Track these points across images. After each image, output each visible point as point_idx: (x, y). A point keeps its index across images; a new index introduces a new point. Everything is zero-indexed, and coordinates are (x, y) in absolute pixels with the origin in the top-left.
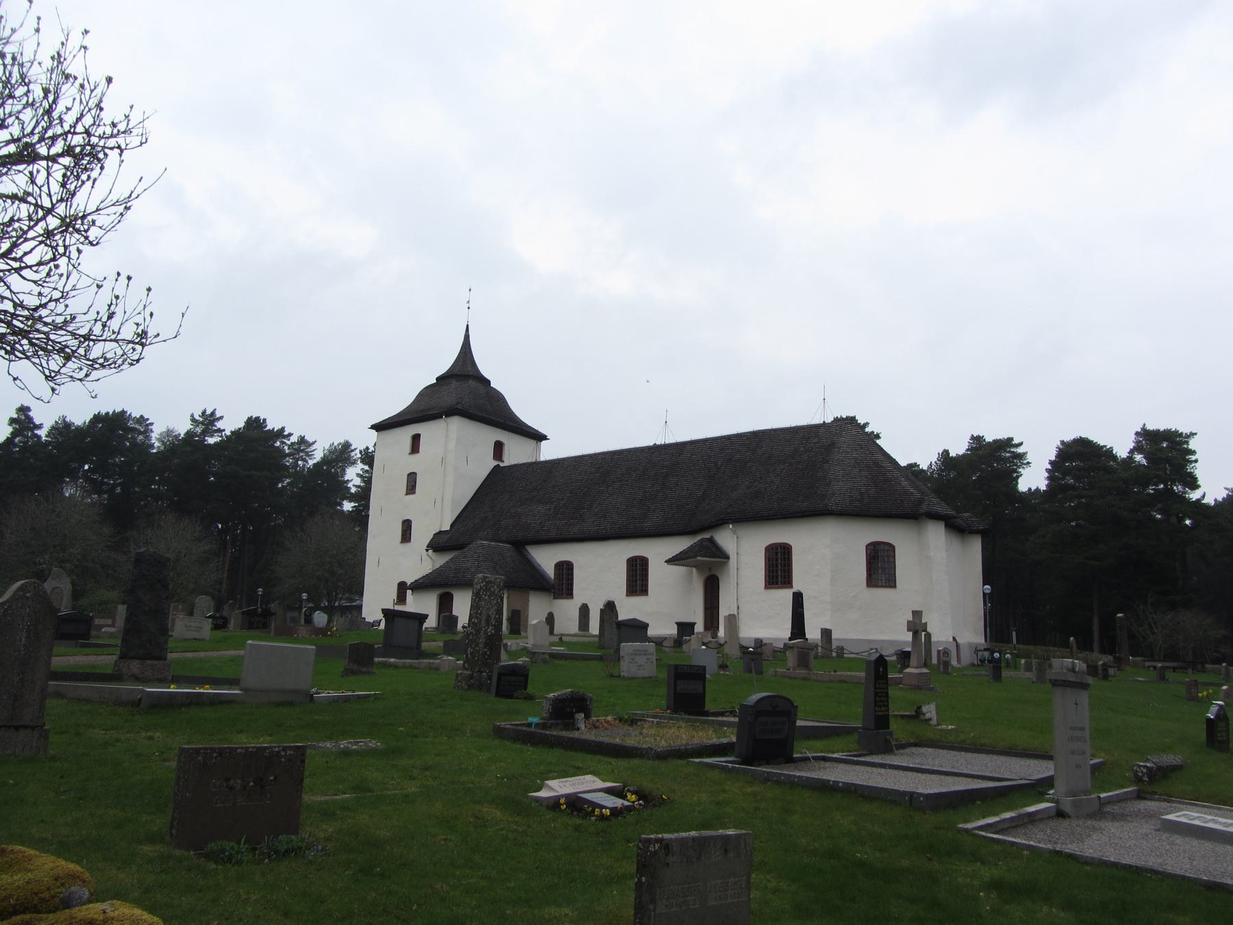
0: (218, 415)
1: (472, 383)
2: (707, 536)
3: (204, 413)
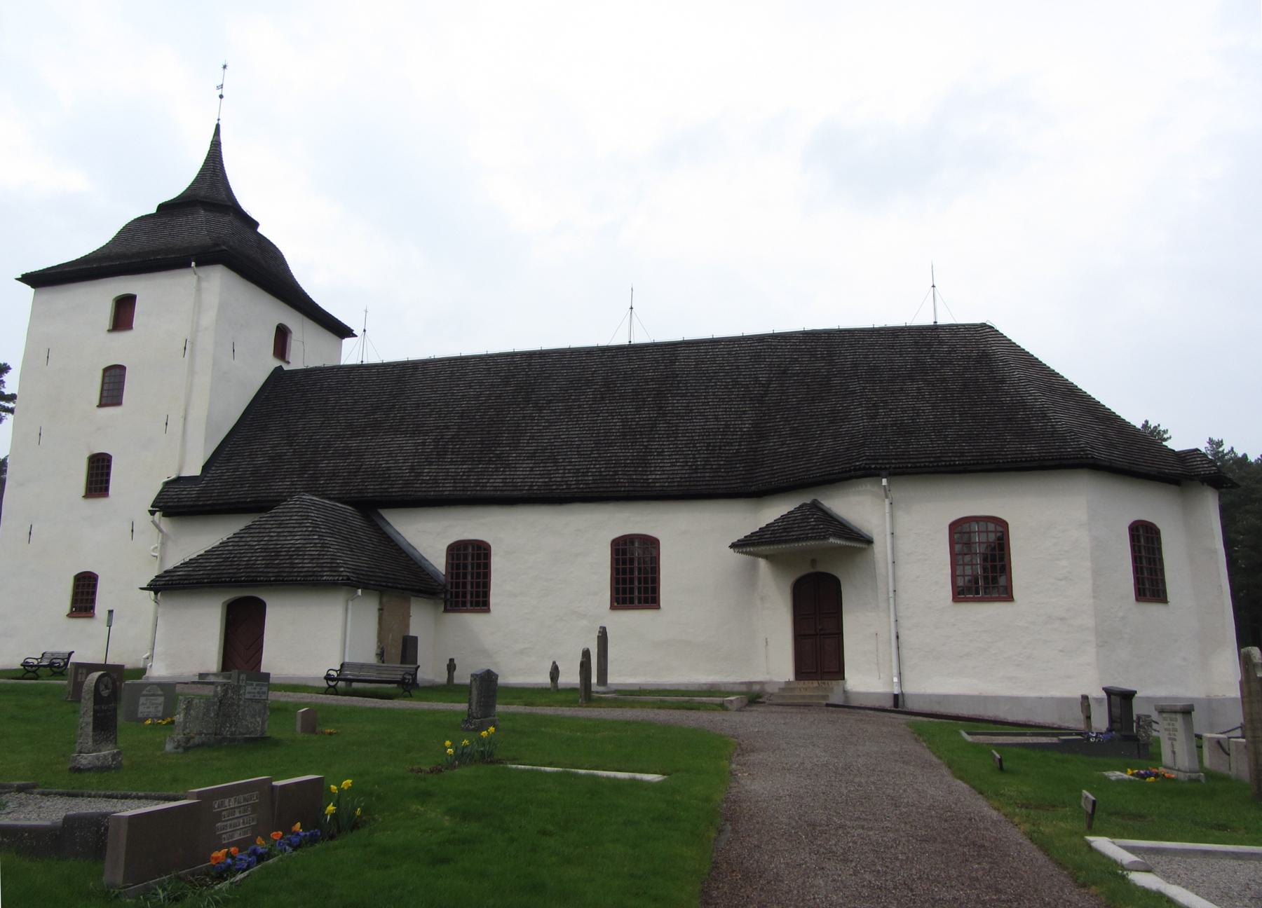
1: (228, 219)
2: (806, 498)
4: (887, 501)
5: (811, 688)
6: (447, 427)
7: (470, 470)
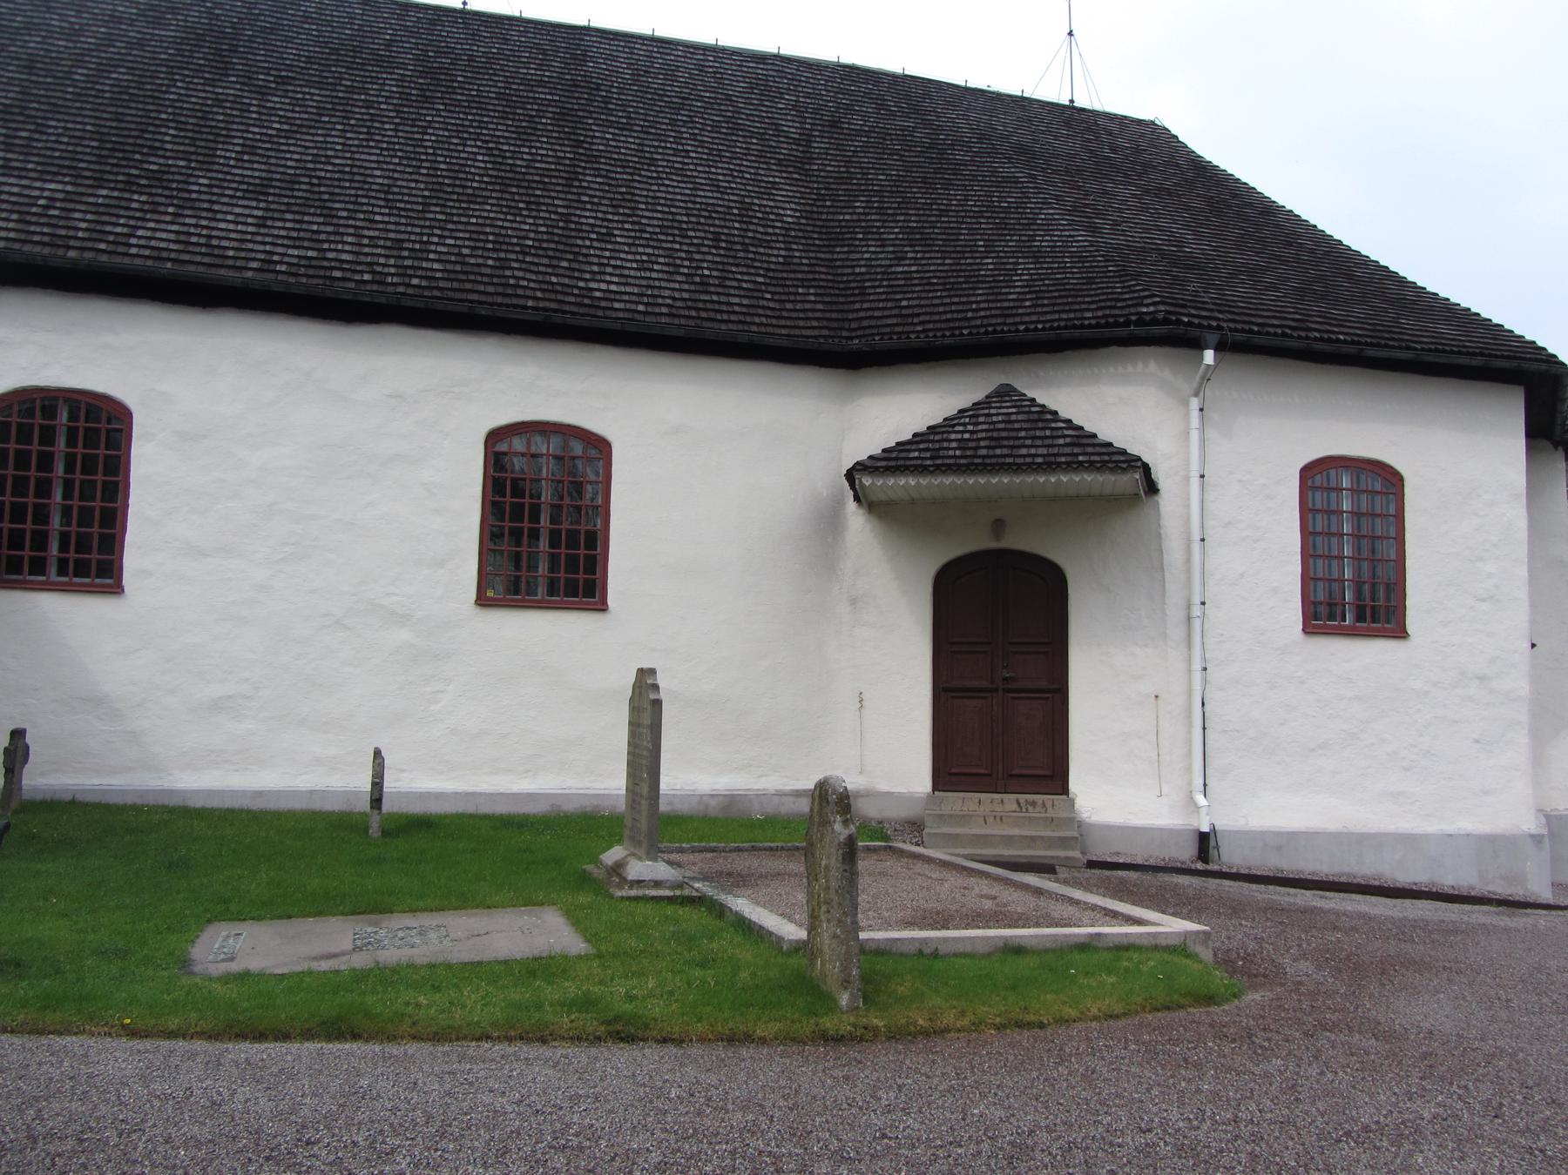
4: (1195, 403)
5: (995, 816)
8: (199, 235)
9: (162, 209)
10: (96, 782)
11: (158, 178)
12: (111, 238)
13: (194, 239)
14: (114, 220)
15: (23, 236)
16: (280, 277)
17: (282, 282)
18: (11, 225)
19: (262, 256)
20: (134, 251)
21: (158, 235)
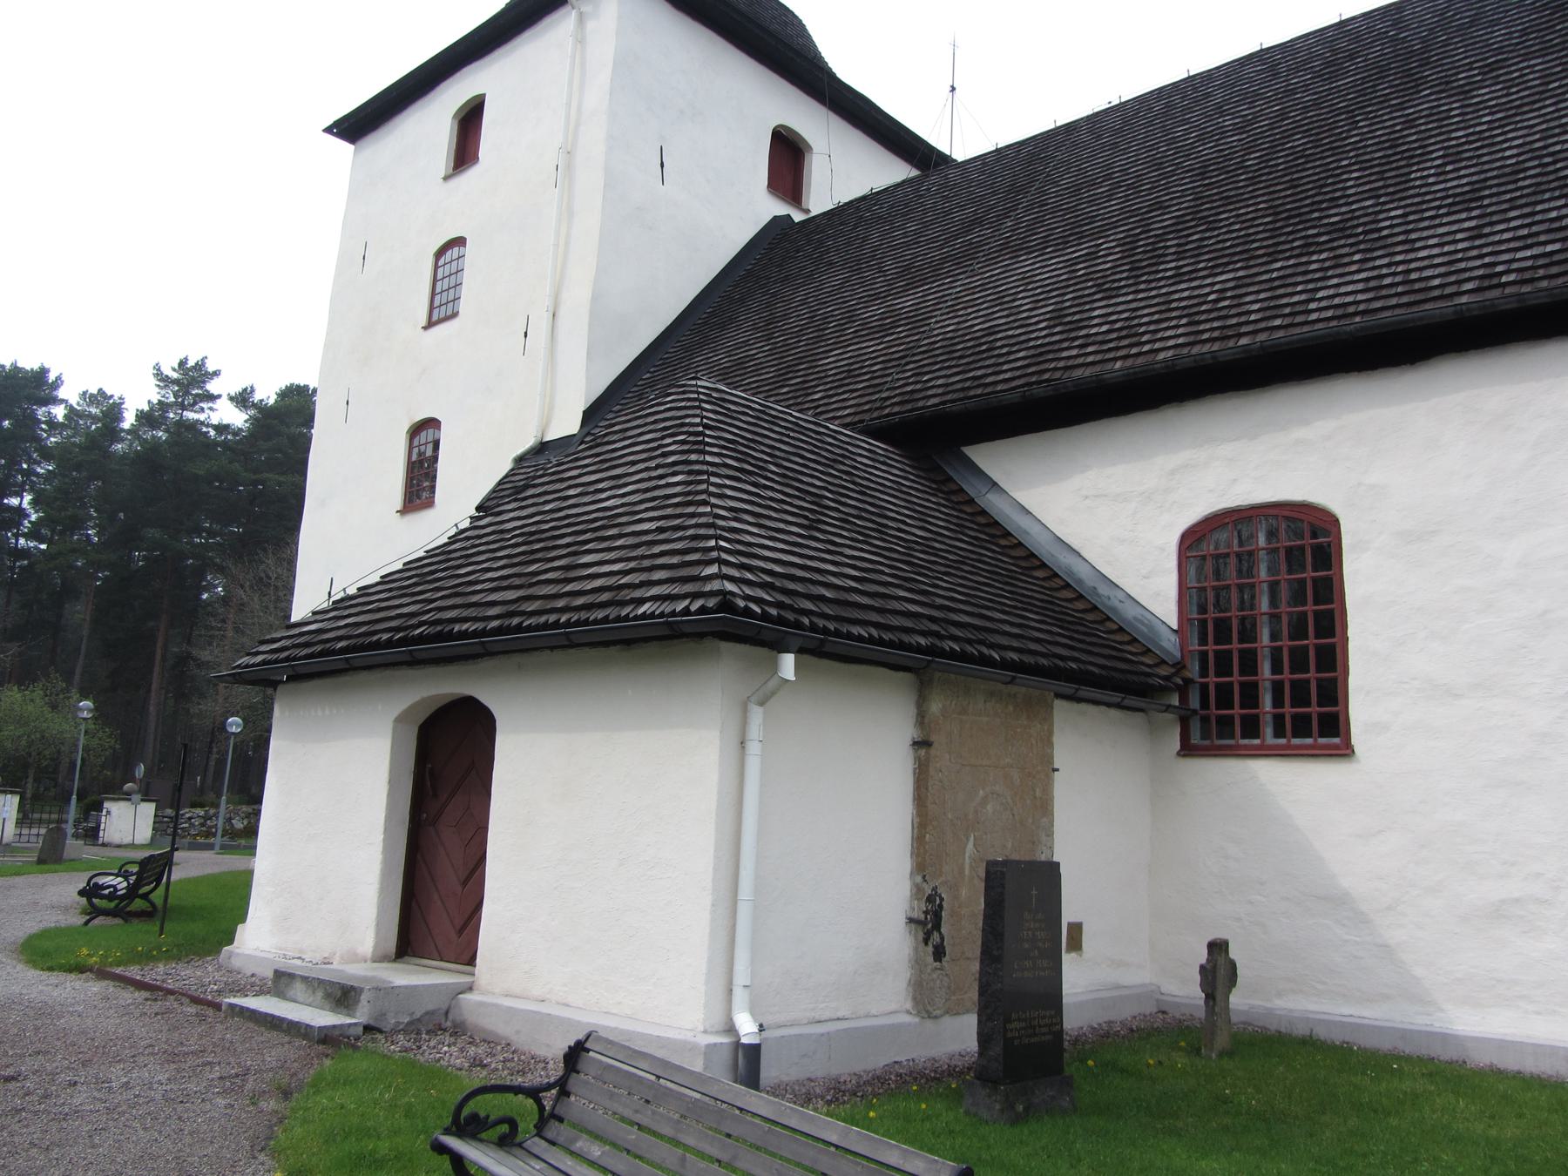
0: (211, 368)
3: (182, 363)
6: (1160, 206)
7: (1240, 283)
8: (1394, 274)
9: (1346, 260)
10: (1346, 1010)
11: (1341, 230)
12: (1287, 310)
13: (1387, 281)
14: (1290, 290)
15: (1192, 339)
16: (1508, 290)
17: (1511, 296)
18: (1180, 331)
19: (1481, 272)
20: (1314, 316)
21: (1343, 290)
